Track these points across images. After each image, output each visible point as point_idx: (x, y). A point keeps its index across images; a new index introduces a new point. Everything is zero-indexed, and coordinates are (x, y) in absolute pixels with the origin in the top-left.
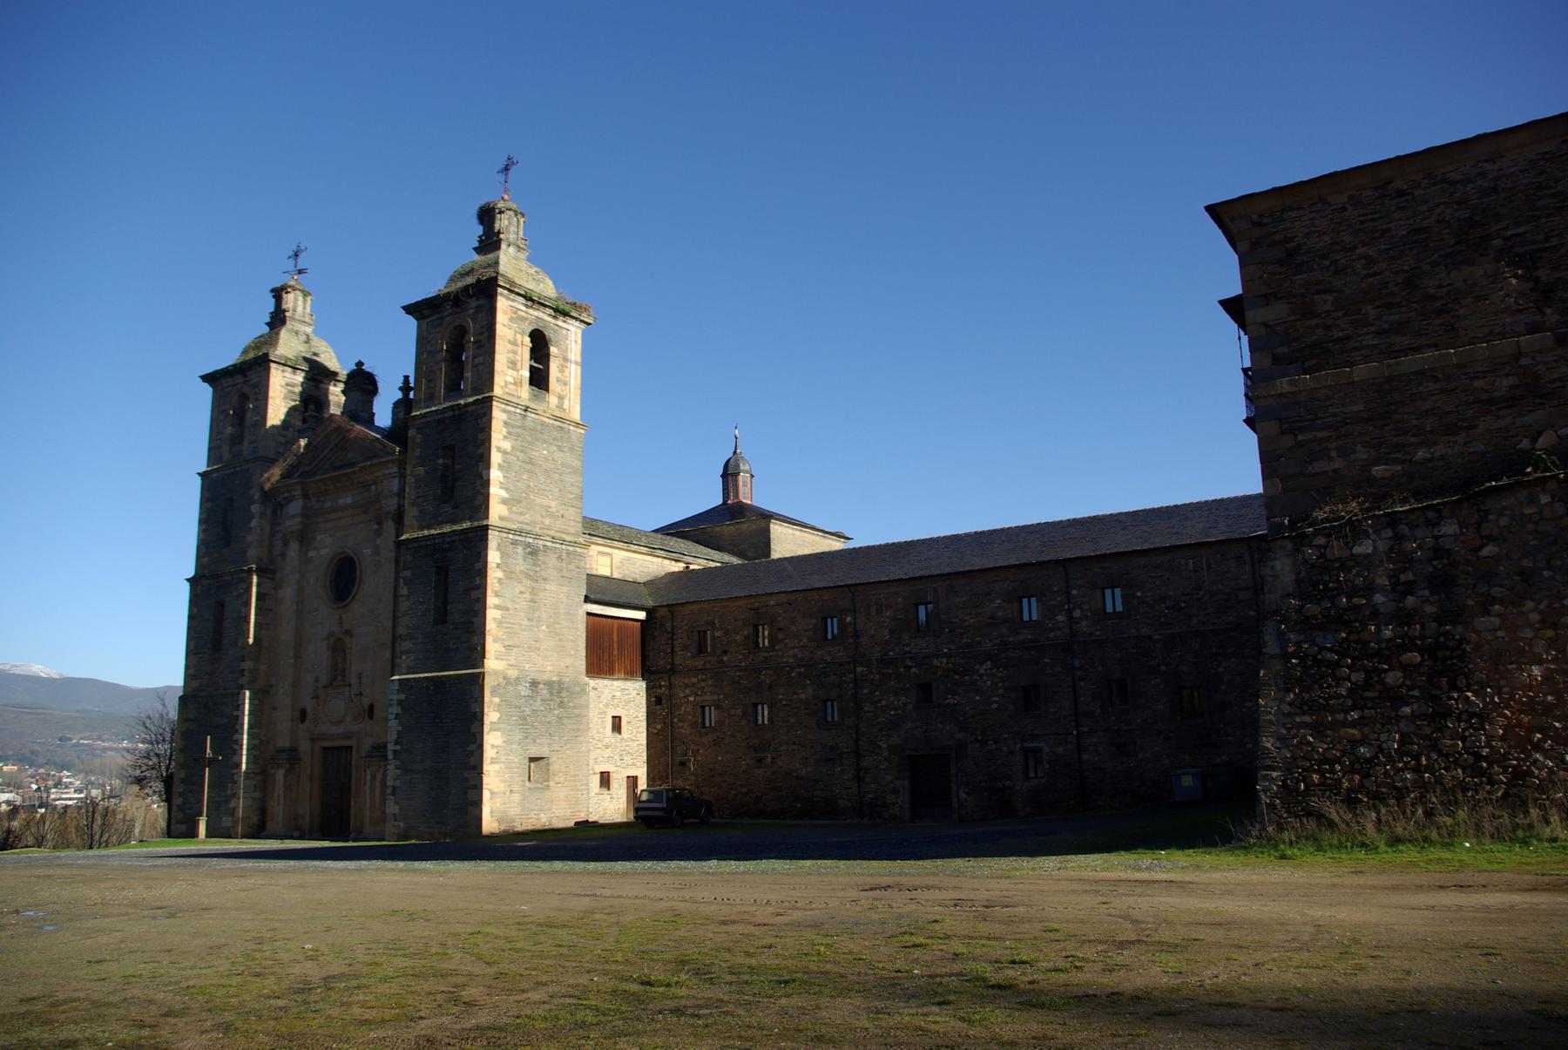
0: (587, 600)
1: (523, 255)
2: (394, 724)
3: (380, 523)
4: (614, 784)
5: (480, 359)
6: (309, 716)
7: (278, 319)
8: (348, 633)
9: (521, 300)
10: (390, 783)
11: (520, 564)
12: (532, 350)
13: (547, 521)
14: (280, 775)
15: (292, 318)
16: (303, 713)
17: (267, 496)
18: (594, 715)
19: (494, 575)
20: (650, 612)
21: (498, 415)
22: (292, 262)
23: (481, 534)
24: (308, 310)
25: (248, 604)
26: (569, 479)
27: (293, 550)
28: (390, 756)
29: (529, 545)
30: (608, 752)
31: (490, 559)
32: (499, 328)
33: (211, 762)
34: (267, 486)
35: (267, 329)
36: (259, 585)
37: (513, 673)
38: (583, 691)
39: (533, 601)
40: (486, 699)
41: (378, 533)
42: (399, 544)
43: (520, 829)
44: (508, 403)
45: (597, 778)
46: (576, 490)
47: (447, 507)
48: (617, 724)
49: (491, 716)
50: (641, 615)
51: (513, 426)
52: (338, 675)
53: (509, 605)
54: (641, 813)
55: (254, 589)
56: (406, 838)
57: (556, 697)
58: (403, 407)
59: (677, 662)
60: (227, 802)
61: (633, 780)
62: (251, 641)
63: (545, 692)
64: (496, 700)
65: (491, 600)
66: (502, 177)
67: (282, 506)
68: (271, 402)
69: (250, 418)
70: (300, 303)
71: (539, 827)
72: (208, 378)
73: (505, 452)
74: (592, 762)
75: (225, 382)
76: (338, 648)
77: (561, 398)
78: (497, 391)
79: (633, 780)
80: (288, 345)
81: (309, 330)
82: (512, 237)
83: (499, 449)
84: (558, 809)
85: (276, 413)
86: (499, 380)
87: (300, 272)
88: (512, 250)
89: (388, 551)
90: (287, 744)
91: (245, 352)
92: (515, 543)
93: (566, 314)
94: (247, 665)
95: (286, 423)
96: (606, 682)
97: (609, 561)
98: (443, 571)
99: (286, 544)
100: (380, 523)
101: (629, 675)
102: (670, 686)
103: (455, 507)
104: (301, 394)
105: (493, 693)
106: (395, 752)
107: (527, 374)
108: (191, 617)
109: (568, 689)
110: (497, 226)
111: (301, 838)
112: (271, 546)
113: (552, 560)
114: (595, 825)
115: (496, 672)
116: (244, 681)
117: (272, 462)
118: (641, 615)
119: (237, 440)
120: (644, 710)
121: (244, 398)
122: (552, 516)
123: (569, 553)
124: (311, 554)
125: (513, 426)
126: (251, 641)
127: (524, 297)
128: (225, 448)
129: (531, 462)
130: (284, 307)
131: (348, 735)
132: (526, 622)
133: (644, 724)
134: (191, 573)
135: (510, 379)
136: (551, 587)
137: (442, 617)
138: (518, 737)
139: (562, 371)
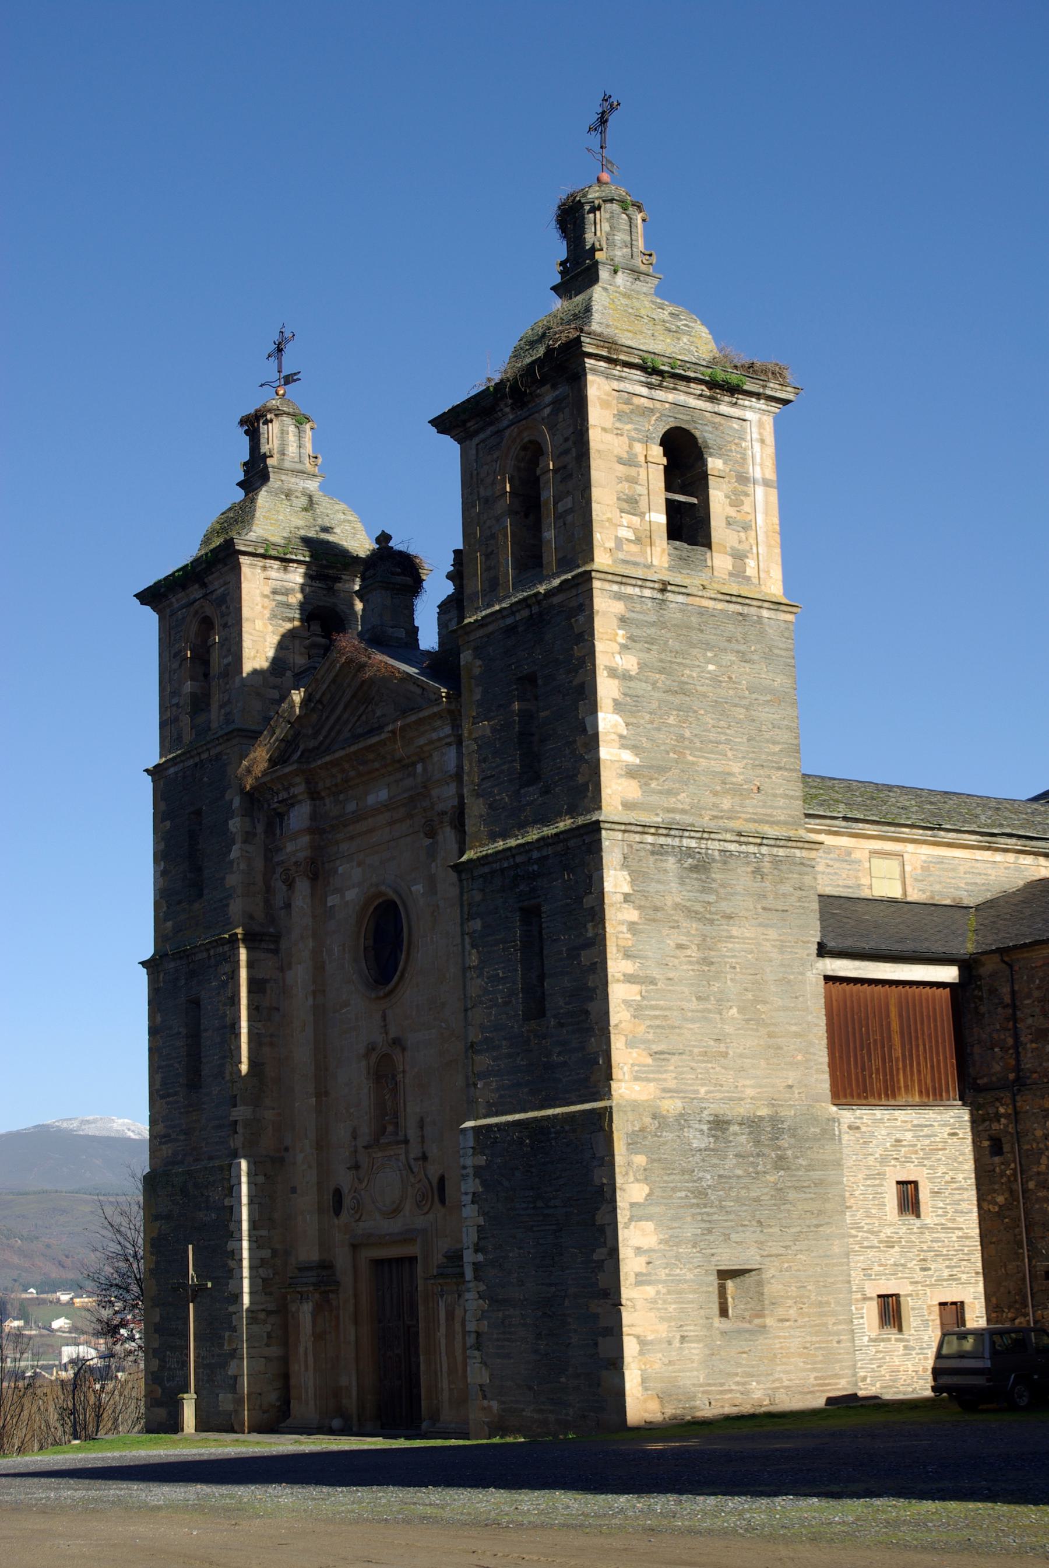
0: (823, 951)
1: (647, 286)
2: (470, 1211)
3: (431, 834)
4: (911, 1320)
5: (568, 503)
6: (347, 1201)
7: (256, 473)
8: (397, 1042)
9: (637, 375)
10: (471, 1326)
11: (672, 888)
12: (667, 470)
13: (726, 803)
14: (305, 1312)
15: (280, 469)
16: (338, 1194)
17: (253, 799)
18: (854, 1180)
19: (620, 918)
20: (966, 966)
21: (607, 606)
22: (273, 363)
23: (587, 843)
24: (309, 448)
25: (235, 1001)
26: (765, 714)
27: (302, 894)
28: (469, 1274)
29: (690, 852)
30: (893, 1255)
31: (608, 886)
32: (596, 437)
33: (199, 1291)
34: (249, 783)
35: (240, 494)
36: (250, 965)
37: (672, 1106)
38: (828, 1133)
39: (707, 961)
40: (619, 1159)
41: (432, 853)
42: (458, 868)
43: (707, 1412)
44: (623, 579)
45: (871, 1310)
46: (785, 736)
47: (532, 793)
48: (909, 1197)
49: (631, 1192)
50: (949, 974)
51: (640, 625)
52: (387, 1124)
53: (655, 973)
54: (945, 1380)
55: (243, 973)
56: (504, 1432)
57: (769, 1147)
58: (451, 609)
59: (1028, 1063)
60: (224, 1365)
61: (953, 1311)
62: (244, 1068)
63: (743, 1140)
64: (640, 1160)
65: (616, 966)
66: (595, 139)
67: (281, 816)
68: (246, 627)
69: (217, 661)
70: (292, 438)
71: (747, 1409)
72: (146, 597)
73: (625, 677)
74: (856, 1276)
75: (177, 600)
76: (384, 1073)
77: (739, 557)
78: (602, 559)
79: (953, 1311)
80: (274, 519)
81: (312, 485)
82: (620, 254)
83: (613, 673)
84: (786, 1371)
85: (259, 643)
86: (602, 539)
87: (288, 380)
88: (621, 279)
89: (448, 885)
90: (315, 1256)
91: (207, 540)
92: (659, 851)
93: (733, 390)
94: (241, 1112)
95: (278, 663)
96: (878, 1113)
97: (892, 869)
98: (530, 915)
99: (290, 884)
100: (431, 834)
101: (932, 1096)
102: (1016, 1116)
103: (546, 791)
104: (302, 606)
105: (633, 1146)
106: (476, 1266)
107: (660, 518)
108: (153, 1031)
109: (793, 1132)
110: (589, 238)
111: (345, 1431)
112: (268, 889)
113: (741, 879)
114: (874, 1403)
115: (635, 1106)
116: (237, 1141)
117: (253, 736)
118: (949, 974)
119: (200, 703)
120: (970, 1165)
121: (207, 624)
122: (737, 791)
123: (776, 861)
124: (332, 900)
125: (640, 625)
126: (244, 1068)
127: (642, 368)
128: (186, 720)
129: (682, 690)
130: (264, 449)
131: (407, 1237)
132: (694, 1004)
133: (972, 1194)
134: (148, 952)
135: (625, 533)
136: (744, 931)
137: (536, 1006)
138: (690, 1230)
139: (736, 504)
